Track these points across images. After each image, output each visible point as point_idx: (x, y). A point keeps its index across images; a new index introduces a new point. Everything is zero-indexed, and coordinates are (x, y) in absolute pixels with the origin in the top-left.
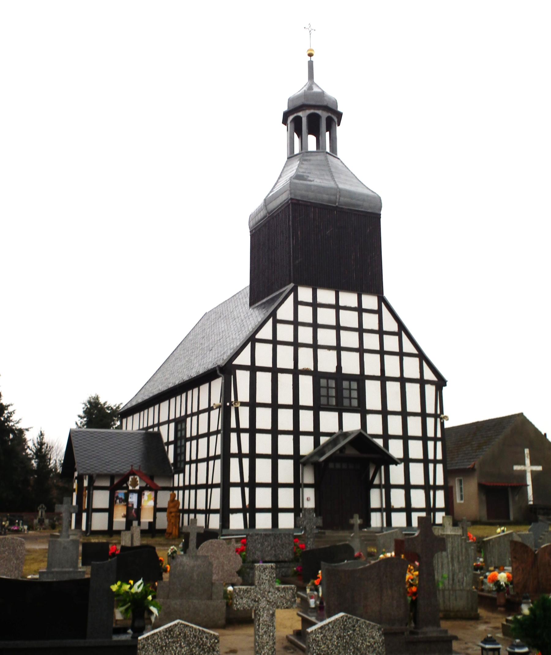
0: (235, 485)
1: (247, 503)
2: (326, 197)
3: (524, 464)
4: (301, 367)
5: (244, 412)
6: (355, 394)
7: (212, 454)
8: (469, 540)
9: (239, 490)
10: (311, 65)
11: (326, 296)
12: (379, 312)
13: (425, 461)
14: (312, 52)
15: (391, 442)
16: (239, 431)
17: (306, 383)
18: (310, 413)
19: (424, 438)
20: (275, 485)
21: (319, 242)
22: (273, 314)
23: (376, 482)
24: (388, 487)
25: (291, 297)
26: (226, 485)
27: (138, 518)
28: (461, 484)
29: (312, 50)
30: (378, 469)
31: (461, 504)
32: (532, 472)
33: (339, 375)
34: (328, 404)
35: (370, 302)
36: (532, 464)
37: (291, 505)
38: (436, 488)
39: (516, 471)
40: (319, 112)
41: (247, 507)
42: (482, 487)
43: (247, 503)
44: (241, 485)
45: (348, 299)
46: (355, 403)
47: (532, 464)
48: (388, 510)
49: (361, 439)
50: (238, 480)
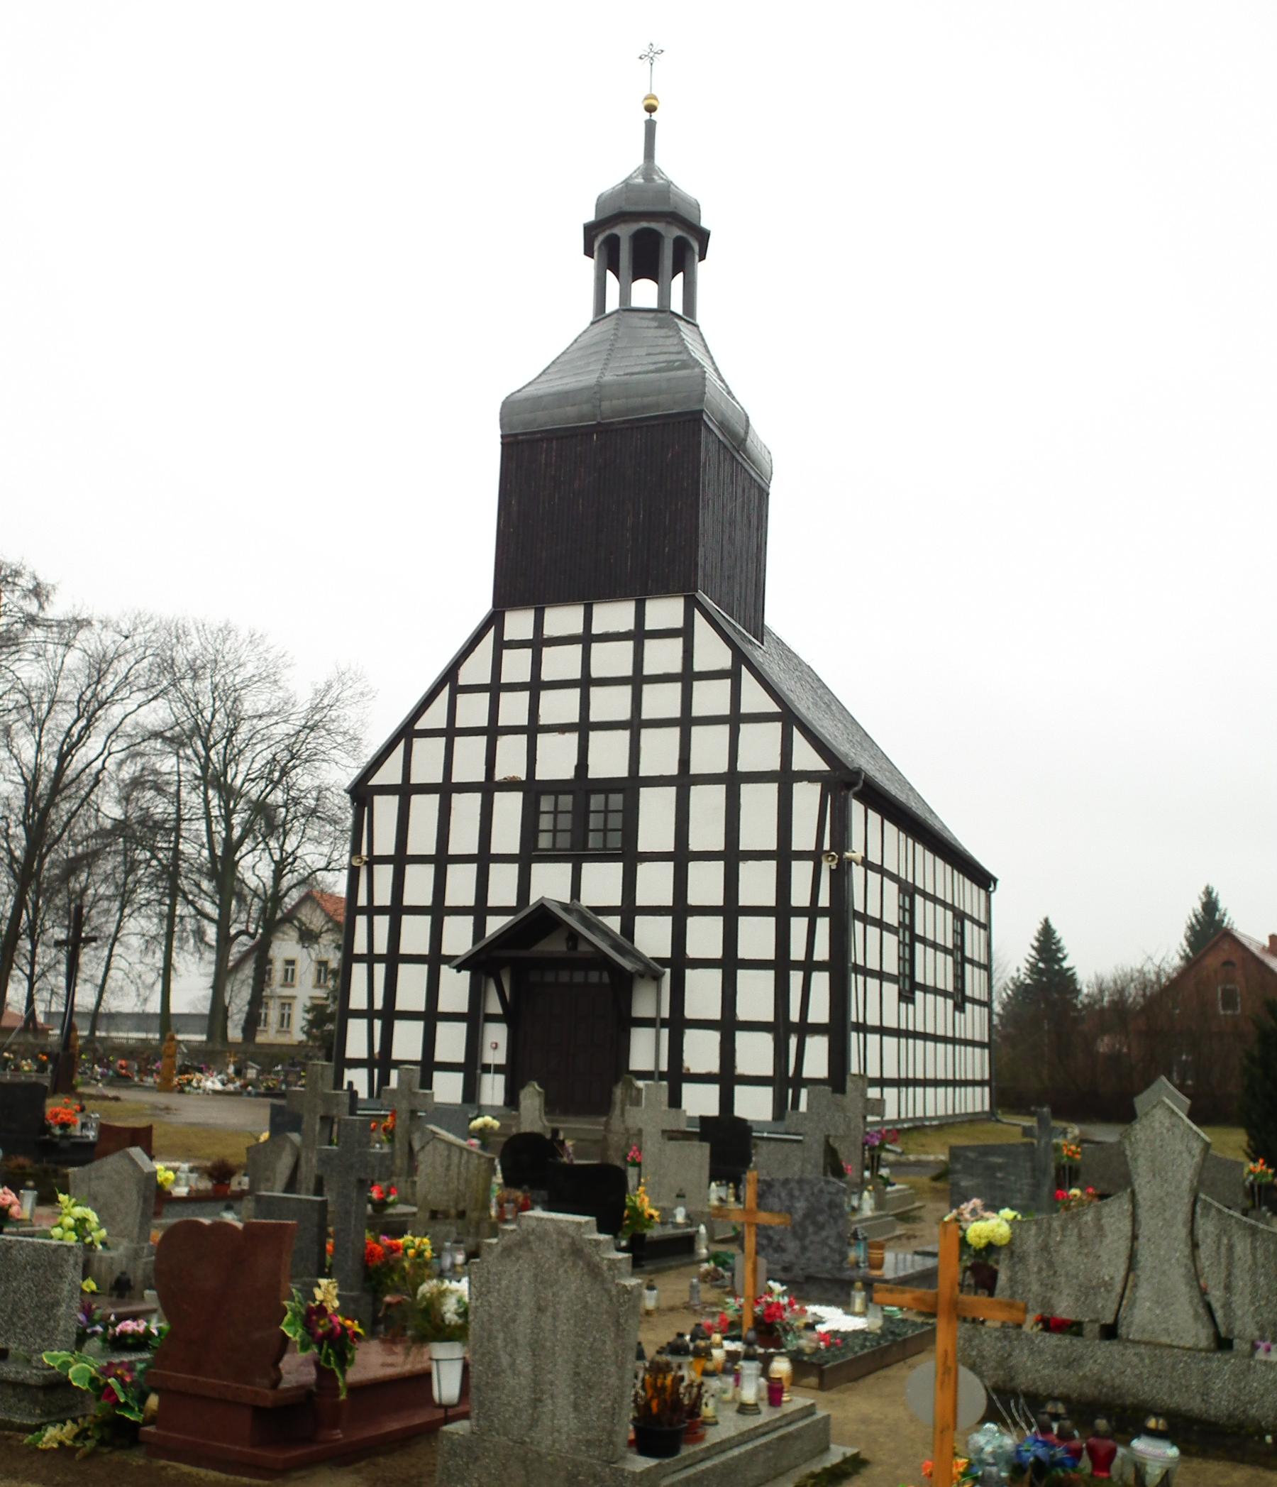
0: (358, 1014)
1: (377, 1049)
2: (571, 411)
6: (545, 822)
9: (363, 1023)
10: (650, 127)
11: (614, 616)
12: (686, 633)
14: (653, 102)
17: (509, 807)
18: (513, 870)
20: (431, 1017)
21: (624, 496)
29: (655, 98)
33: (582, 784)
34: (605, 848)
37: (460, 1057)
38: (805, 1029)
41: (377, 1057)
43: (377, 1049)
44: (369, 1014)
50: (363, 1005)
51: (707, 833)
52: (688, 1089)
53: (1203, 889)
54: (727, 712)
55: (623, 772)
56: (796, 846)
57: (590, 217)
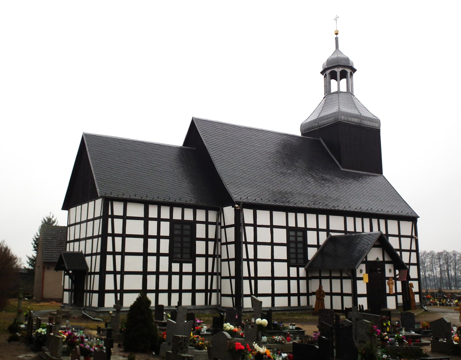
0: (110, 273)
7: (94, 251)
10: (337, 39)
15: (403, 253)
33: (182, 222)
40: (347, 70)
44: (249, 278)
54: (258, 276)
55: (285, 230)
56: (149, 270)
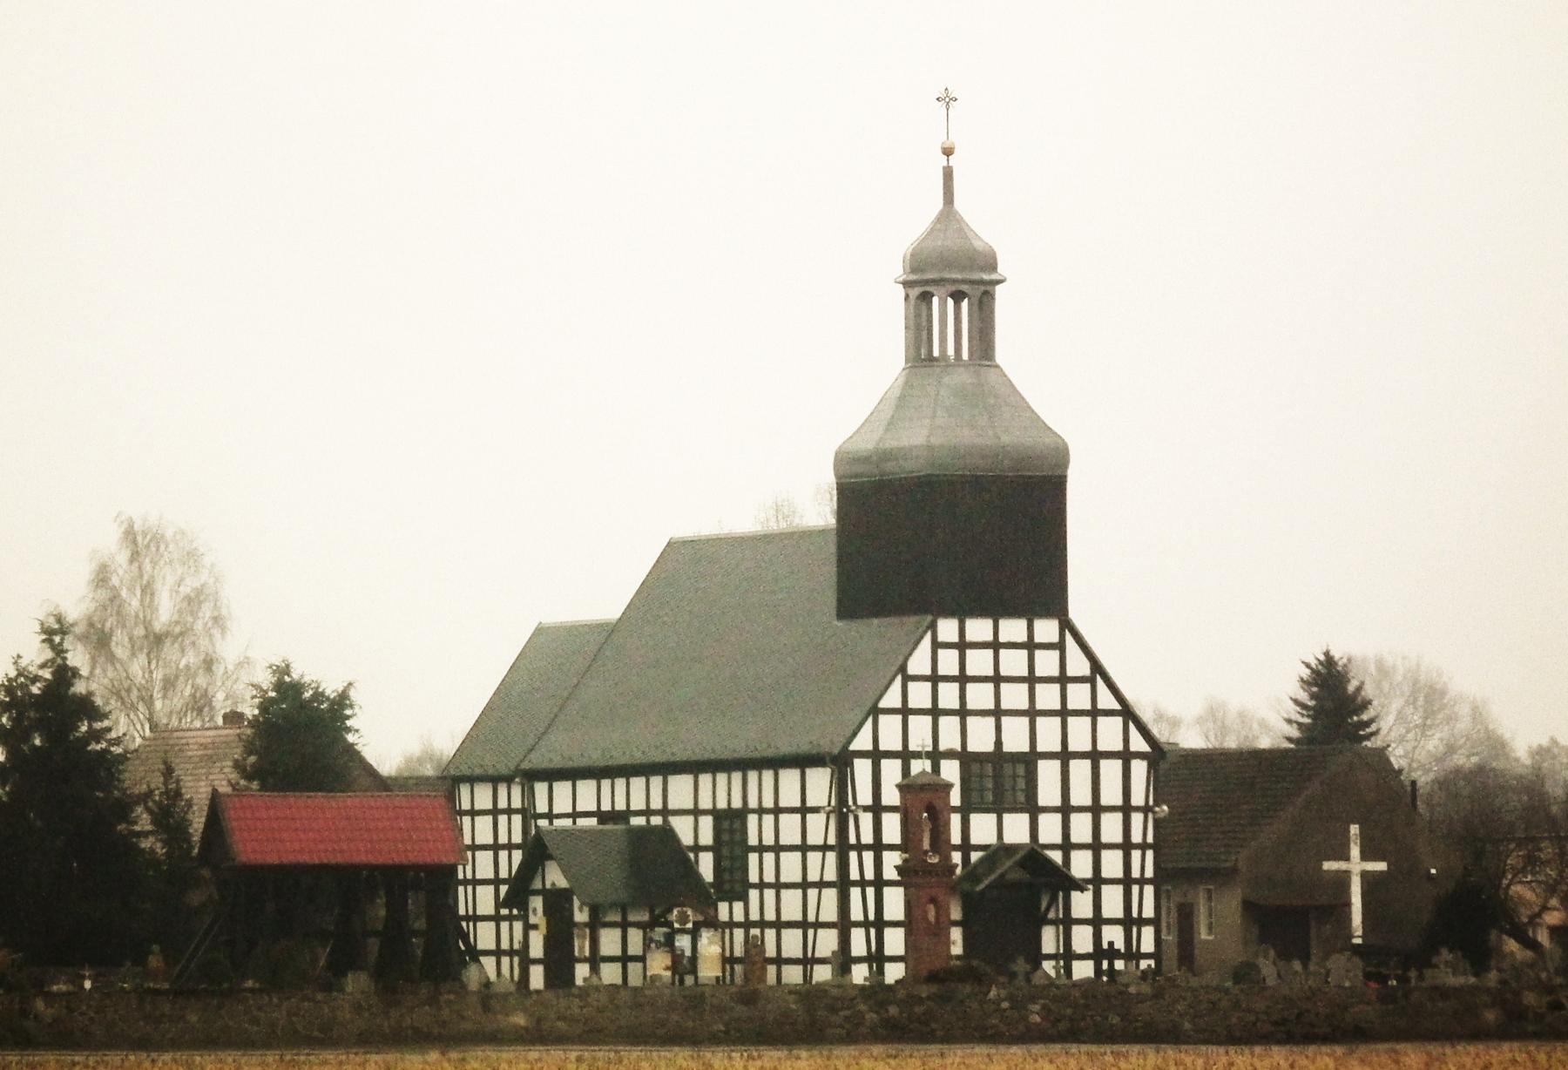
0: (857, 924)
3: (1347, 859)
4: (942, 747)
5: (866, 820)
6: (1021, 783)
8: (98, 742)
10: (948, 174)
11: (979, 629)
12: (1060, 646)
13: (1127, 881)
15: (491, 911)
16: (860, 848)
19: (1126, 846)
22: (903, 669)
23: (1051, 915)
24: (1068, 922)
25: (929, 635)
26: (844, 925)
27: (694, 970)
28: (1210, 899)
30: (1054, 899)
31: (1207, 942)
32: (1365, 875)
33: (999, 756)
35: (1047, 629)
36: (1365, 857)
38: (1142, 922)
39: (1328, 872)
42: (1248, 906)
44: (866, 924)
45: (1013, 629)
46: (1021, 798)
47: (1365, 857)
48: (1067, 956)
49: (1032, 856)
50: (861, 918)
51: (1081, 794)
52: (1076, 964)
53: (350, 679)
55: (1026, 749)
57: (1336, 654)
